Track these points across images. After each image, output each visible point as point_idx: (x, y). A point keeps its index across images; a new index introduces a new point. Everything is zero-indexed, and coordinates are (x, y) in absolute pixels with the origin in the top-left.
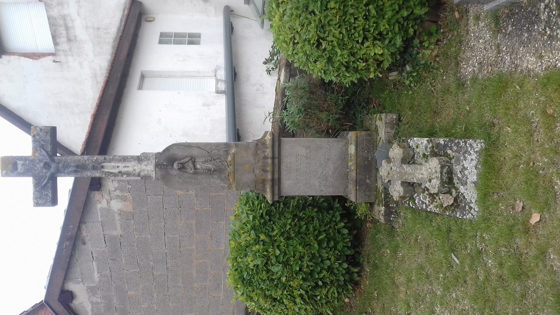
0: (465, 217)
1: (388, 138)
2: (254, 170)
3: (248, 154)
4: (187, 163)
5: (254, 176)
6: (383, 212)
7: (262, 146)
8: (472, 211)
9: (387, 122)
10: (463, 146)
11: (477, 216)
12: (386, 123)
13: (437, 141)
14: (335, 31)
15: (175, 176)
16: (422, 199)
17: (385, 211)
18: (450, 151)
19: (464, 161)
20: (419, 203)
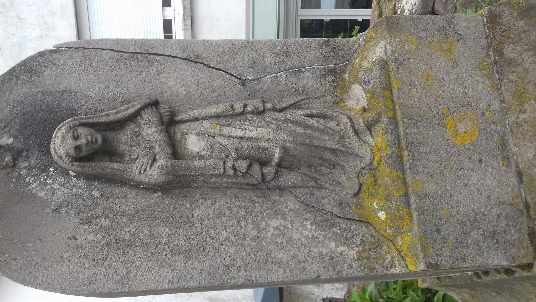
2: (503, 147)
3: (456, 65)
4: (131, 128)
5: (514, 180)
7: (521, 24)
14: (271, 234)
15: (57, 210)
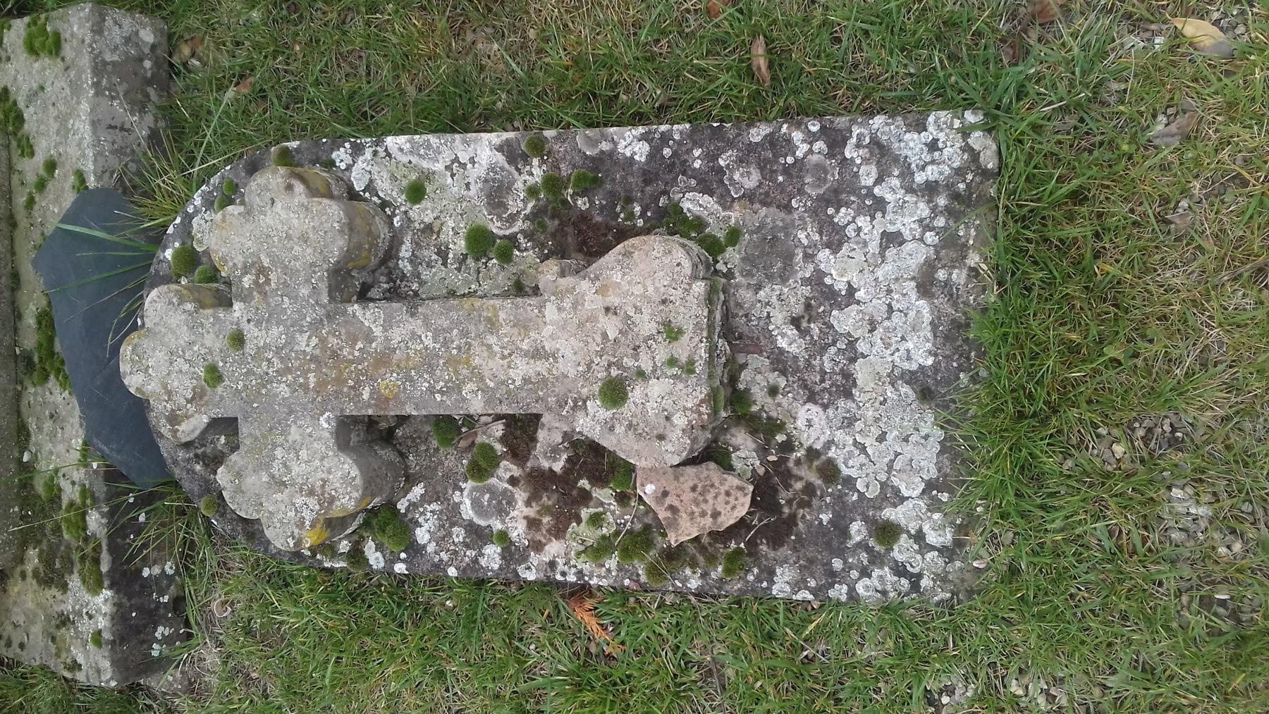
0: (839, 592)
1: (114, 163)
6: (102, 623)
8: (903, 551)
9: (108, 57)
10: (815, 158)
11: (942, 578)
12: (100, 68)
13: (593, 143)
16: (467, 511)
17: (120, 617)
18: (706, 200)
19: (824, 254)
20: (442, 538)
